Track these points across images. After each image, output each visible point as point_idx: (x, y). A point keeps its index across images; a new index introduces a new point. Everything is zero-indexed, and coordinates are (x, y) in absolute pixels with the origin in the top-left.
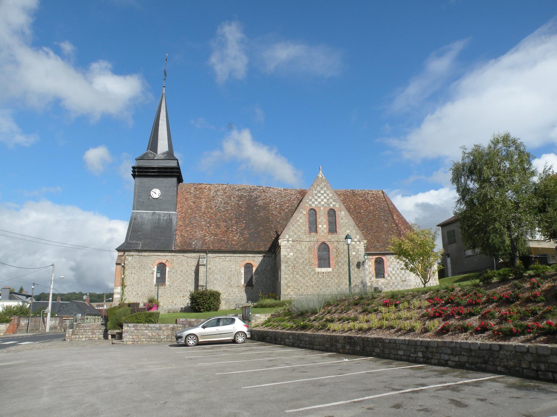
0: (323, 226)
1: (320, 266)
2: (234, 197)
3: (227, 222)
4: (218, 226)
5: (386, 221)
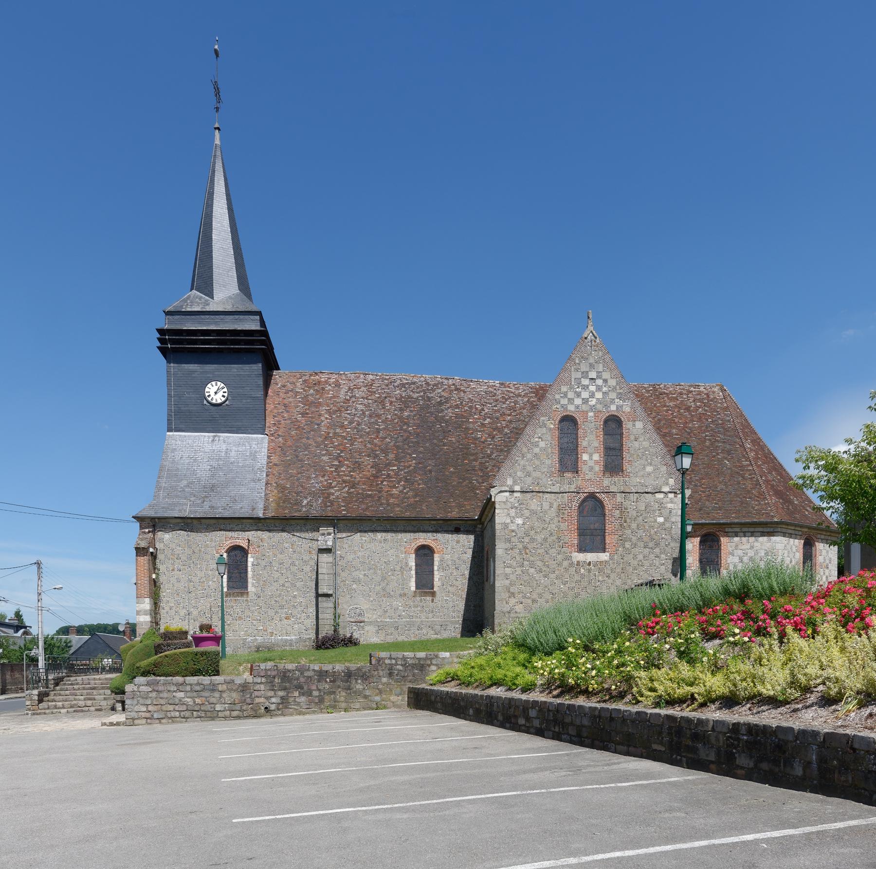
0: (591, 457)
1: (582, 549)
2: (391, 403)
3: (376, 456)
4: (358, 466)
5: (729, 452)
